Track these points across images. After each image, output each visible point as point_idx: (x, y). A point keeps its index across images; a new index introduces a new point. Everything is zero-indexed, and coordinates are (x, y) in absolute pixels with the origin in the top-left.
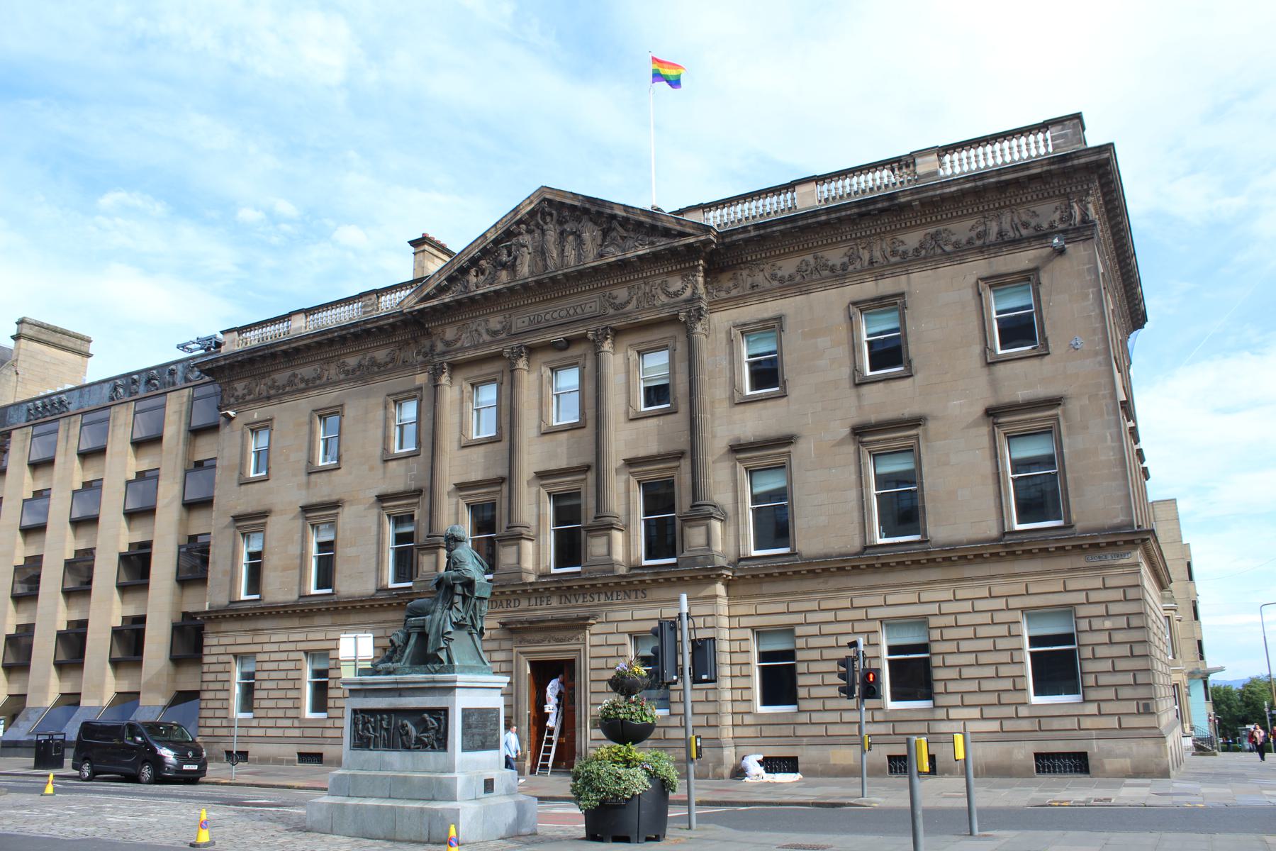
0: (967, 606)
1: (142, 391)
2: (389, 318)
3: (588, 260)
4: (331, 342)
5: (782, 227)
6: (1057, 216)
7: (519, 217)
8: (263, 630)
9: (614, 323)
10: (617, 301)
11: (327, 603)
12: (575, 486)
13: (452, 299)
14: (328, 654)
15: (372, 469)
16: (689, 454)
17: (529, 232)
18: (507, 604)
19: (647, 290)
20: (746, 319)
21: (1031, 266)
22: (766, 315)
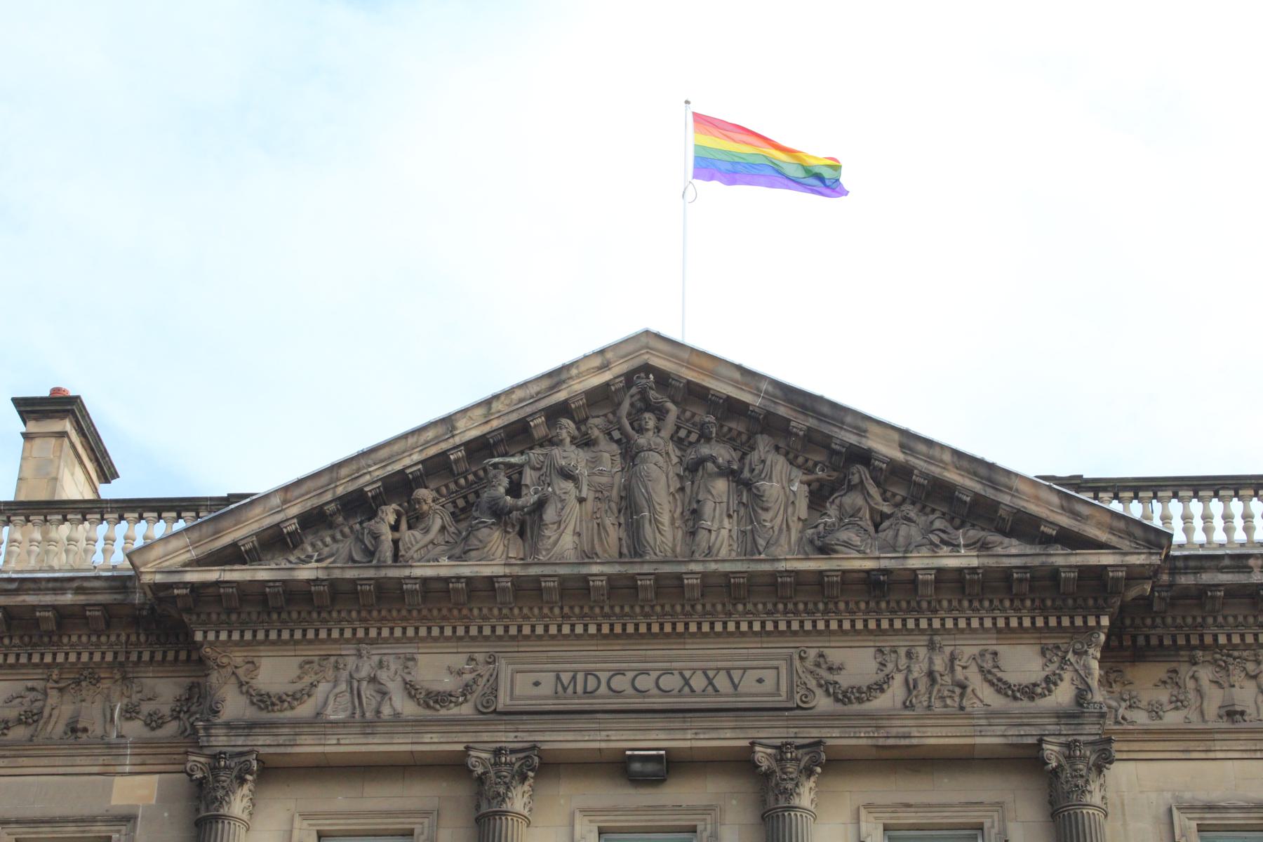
7: (561, 396)
9: (836, 738)
10: (844, 680)
13: (321, 575)
17: (586, 442)
19: (939, 664)
20: (1216, 795)
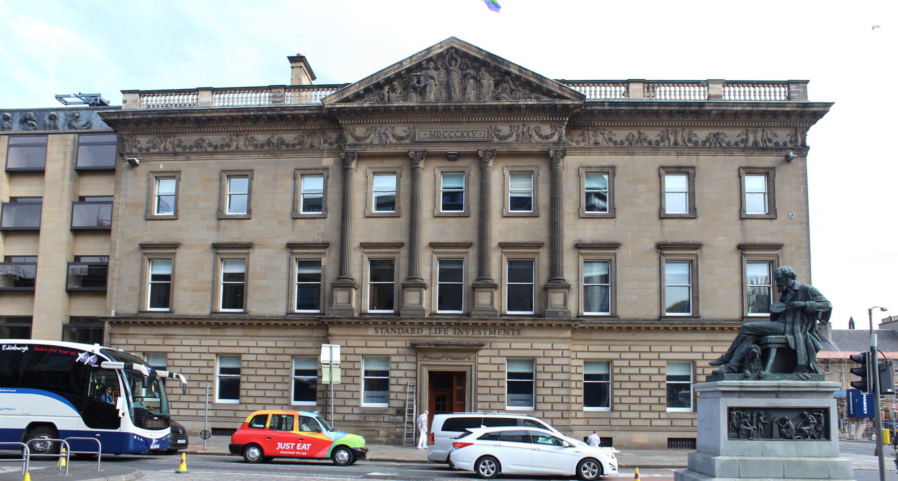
0: (636, 356)
1: (16, 127)
2: (305, 110)
3: (486, 99)
4: (245, 119)
5: (627, 108)
6: (788, 139)
7: (430, 55)
8: (174, 335)
9: (499, 149)
10: (501, 134)
11: (242, 320)
12: (461, 256)
13: (370, 105)
14: (166, 356)
15: (281, 223)
16: (407, 246)
17: (436, 69)
18: (412, 331)
21: (771, 165)
22: (603, 164)
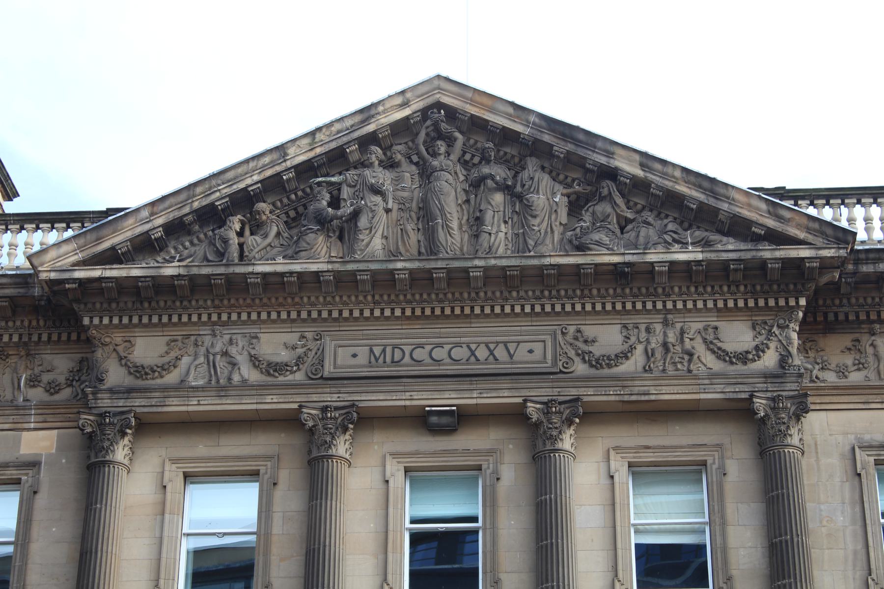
3: (546, 249)
7: (371, 128)
9: (591, 395)
10: (597, 350)
17: (390, 165)
